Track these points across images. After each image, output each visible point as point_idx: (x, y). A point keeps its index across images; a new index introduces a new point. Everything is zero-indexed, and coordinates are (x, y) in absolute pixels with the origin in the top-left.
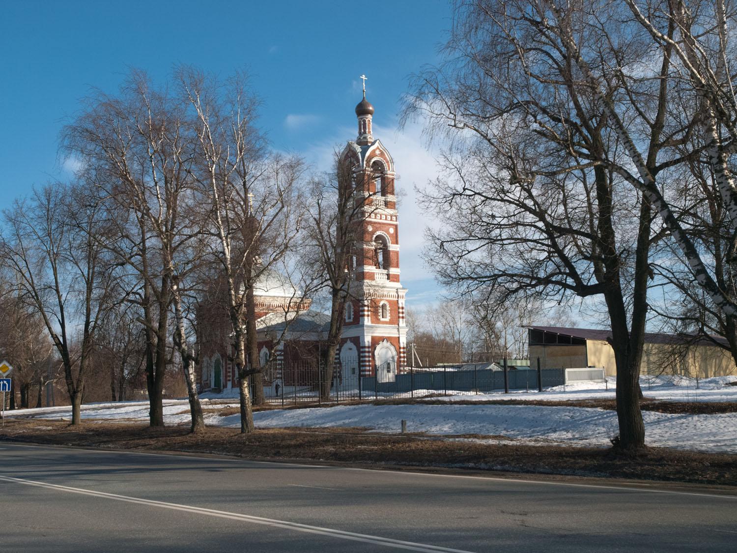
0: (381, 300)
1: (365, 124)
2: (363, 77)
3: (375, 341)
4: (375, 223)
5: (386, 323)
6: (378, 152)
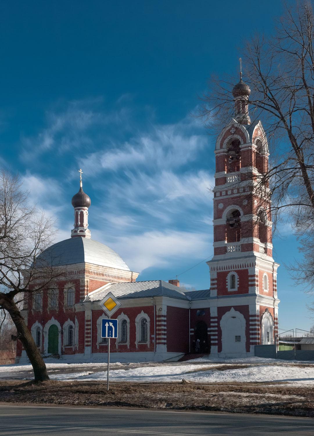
5: (235, 293)
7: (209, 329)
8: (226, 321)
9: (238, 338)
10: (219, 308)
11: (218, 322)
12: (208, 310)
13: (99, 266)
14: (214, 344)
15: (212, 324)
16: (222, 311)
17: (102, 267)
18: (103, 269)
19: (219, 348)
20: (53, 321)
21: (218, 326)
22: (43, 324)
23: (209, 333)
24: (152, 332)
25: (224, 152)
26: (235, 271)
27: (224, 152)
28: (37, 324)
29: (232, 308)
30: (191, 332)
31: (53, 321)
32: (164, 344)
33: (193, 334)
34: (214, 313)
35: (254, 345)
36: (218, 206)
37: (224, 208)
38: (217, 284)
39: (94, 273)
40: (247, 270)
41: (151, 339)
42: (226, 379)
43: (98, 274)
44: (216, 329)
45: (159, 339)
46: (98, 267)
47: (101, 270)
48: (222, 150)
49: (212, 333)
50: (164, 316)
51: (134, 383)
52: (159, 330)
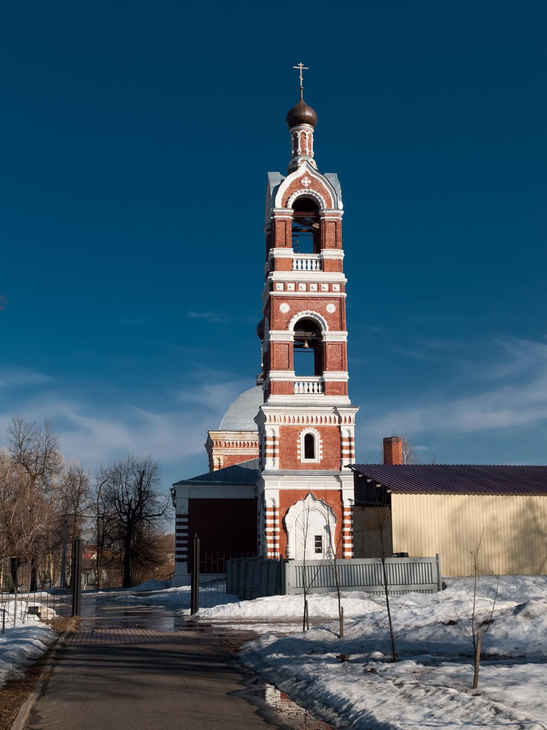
0: (302, 428)
1: (296, 140)
2: (301, 66)
3: (289, 498)
4: (295, 298)
5: (314, 466)
6: (306, 182)
8: (295, 515)
13: (242, 433)
16: (289, 498)
17: (251, 433)
18: (253, 435)
19: (188, 565)
26: (318, 428)
39: (235, 444)
42: (425, 616)
46: (241, 434)
51: (358, 617)
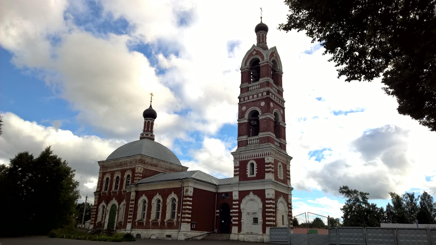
5: (253, 179)
7: (231, 211)
9: (255, 220)
10: (240, 192)
11: (239, 205)
12: (231, 193)
14: (235, 225)
15: (234, 207)
16: (243, 194)
20: (114, 202)
21: (239, 209)
22: (107, 204)
23: (231, 215)
24: (179, 212)
25: (247, 69)
27: (247, 69)
28: (103, 203)
29: (251, 193)
30: (217, 213)
31: (114, 202)
32: (188, 222)
33: (218, 215)
34: (236, 196)
35: (269, 227)
36: (242, 108)
37: (246, 110)
38: (239, 171)
40: (264, 158)
41: (178, 217)
43: (152, 165)
44: (237, 210)
45: (184, 218)
47: (155, 162)
48: (246, 67)
49: (233, 214)
50: (190, 197)
52: (185, 209)
